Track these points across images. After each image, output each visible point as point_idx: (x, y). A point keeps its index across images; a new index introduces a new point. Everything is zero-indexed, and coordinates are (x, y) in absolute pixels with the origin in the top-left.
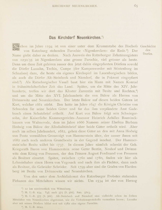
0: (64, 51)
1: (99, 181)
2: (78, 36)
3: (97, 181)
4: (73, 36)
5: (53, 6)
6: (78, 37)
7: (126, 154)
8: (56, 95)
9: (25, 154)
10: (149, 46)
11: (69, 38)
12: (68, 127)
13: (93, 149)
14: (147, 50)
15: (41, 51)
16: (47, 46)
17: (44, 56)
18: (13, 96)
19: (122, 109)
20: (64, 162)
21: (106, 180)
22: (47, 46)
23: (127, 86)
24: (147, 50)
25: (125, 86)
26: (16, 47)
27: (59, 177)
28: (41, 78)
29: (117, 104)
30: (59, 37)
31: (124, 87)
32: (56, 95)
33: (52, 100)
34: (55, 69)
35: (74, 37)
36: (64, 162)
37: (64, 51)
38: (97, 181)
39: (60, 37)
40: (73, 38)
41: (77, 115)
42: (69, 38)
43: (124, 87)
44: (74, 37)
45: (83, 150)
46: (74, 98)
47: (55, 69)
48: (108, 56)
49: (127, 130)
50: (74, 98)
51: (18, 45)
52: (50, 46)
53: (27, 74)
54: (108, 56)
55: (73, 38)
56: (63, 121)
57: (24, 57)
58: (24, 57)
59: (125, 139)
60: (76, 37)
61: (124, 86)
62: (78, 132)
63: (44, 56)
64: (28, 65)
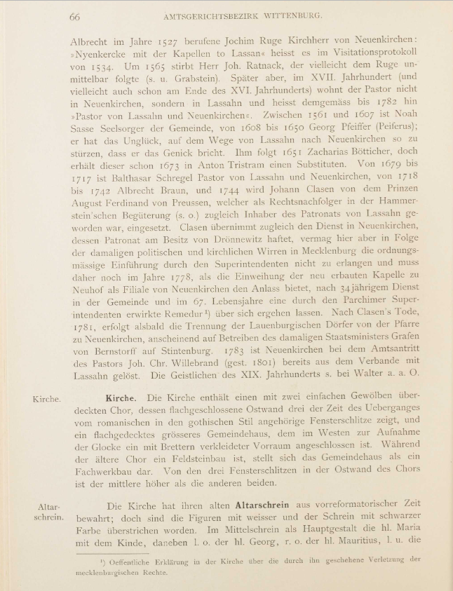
0: (335, 301)
1: (101, 67)
3: (162, 42)
7: (392, 189)
10: (342, 237)
12: (389, 349)
17: (412, 139)
19: (259, 290)
20: (171, 471)
21: (99, 177)
28: (360, 126)
29: (108, 411)
33: (366, 140)
34: (370, 301)
36: (171, 471)
37: (335, 301)
38: (162, 42)
41: (171, 403)
47: (370, 301)
48: (270, 315)
49: (383, 199)
53: (178, 216)
54: (270, 315)
56: (323, 58)
59: (383, 199)
61: (248, 374)
62: (231, 290)
63: (412, 139)
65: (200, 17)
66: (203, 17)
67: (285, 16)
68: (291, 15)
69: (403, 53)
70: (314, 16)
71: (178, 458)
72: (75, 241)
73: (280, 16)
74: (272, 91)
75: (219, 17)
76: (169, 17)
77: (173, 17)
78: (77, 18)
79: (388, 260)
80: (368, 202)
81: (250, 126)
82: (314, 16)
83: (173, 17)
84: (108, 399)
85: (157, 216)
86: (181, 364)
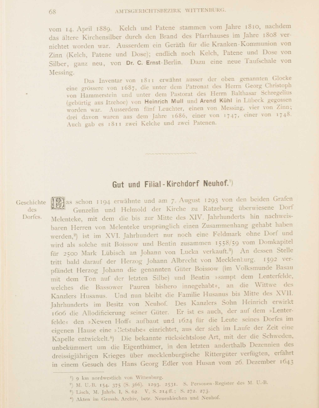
1: (222, 243)
2: (205, 181)
3: (218, 243)
4: (196, 182)
5: (142, 123)
6: (206, 183)
8: (281, 293)
9: (75, 280)
11: (188, 184)
13: (197, 268)
14: (30, 210)
15: (222, 209)
16: (99, 202)
18: (54, 349)
22: (99, 202)
23: (200, 216)
24: (30, 210)
25: (197, 216)
26: (58, 203)
27: (213, 338)
30: (168, 184)
31: (194, 218)
32: (281, 293)
35: (197, 182)
36: (241, 267)
38: (218, 243)
39: (171, 184)
40: (195, 185)
42: (188, 184)
43: (194, 218)
44: (197, 182)
45: (177, 270)
46: (128, 232)
49: (83, 295)
50: (128, 232)
51: (59, 199)
52: (105, 202)
55: (195, 185)
57: (142, 272)
58: (142, 272)
60: (201, 183)
61: (194, 217)
64: (252, 337)
65: (140, 11)
66: (142, 11)
67: (200, 10)
68: (204, 10)
69: (176, 339)
70: (220, 10)
71: (217, 234)
72: (55, 356)
73: (197, 11)
74: (219, 218)
75: (154, 11)
76: (119, 11)
77: (122, 11)
78: (64, 314)
79: (290, 231)
80: (120, 279)
81: (58, 312)
82: (220, 10)
83: (122, 11)
84: (121, 29)
85: (116, 313)
86: (262, 285)
